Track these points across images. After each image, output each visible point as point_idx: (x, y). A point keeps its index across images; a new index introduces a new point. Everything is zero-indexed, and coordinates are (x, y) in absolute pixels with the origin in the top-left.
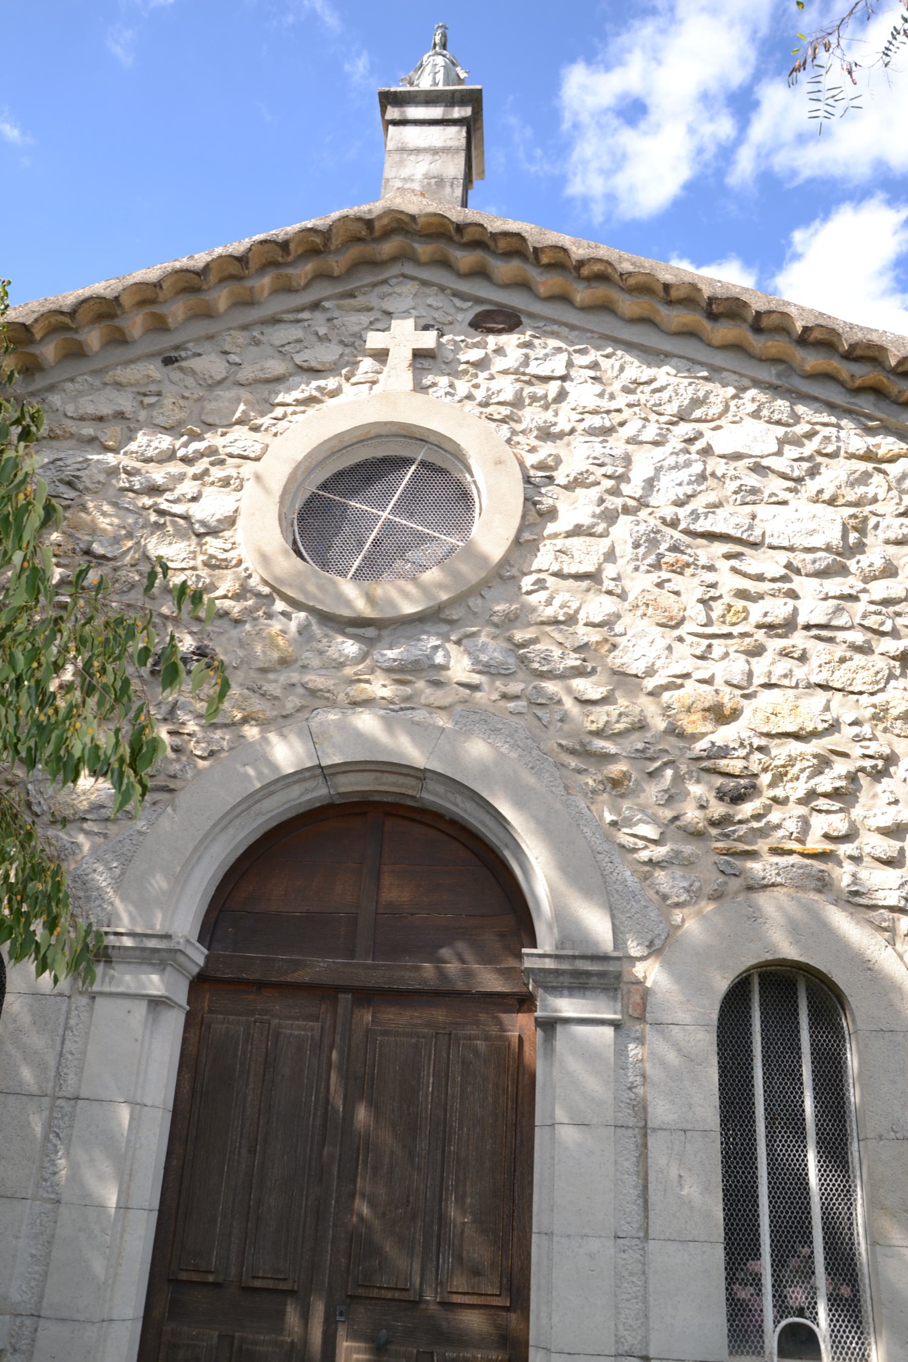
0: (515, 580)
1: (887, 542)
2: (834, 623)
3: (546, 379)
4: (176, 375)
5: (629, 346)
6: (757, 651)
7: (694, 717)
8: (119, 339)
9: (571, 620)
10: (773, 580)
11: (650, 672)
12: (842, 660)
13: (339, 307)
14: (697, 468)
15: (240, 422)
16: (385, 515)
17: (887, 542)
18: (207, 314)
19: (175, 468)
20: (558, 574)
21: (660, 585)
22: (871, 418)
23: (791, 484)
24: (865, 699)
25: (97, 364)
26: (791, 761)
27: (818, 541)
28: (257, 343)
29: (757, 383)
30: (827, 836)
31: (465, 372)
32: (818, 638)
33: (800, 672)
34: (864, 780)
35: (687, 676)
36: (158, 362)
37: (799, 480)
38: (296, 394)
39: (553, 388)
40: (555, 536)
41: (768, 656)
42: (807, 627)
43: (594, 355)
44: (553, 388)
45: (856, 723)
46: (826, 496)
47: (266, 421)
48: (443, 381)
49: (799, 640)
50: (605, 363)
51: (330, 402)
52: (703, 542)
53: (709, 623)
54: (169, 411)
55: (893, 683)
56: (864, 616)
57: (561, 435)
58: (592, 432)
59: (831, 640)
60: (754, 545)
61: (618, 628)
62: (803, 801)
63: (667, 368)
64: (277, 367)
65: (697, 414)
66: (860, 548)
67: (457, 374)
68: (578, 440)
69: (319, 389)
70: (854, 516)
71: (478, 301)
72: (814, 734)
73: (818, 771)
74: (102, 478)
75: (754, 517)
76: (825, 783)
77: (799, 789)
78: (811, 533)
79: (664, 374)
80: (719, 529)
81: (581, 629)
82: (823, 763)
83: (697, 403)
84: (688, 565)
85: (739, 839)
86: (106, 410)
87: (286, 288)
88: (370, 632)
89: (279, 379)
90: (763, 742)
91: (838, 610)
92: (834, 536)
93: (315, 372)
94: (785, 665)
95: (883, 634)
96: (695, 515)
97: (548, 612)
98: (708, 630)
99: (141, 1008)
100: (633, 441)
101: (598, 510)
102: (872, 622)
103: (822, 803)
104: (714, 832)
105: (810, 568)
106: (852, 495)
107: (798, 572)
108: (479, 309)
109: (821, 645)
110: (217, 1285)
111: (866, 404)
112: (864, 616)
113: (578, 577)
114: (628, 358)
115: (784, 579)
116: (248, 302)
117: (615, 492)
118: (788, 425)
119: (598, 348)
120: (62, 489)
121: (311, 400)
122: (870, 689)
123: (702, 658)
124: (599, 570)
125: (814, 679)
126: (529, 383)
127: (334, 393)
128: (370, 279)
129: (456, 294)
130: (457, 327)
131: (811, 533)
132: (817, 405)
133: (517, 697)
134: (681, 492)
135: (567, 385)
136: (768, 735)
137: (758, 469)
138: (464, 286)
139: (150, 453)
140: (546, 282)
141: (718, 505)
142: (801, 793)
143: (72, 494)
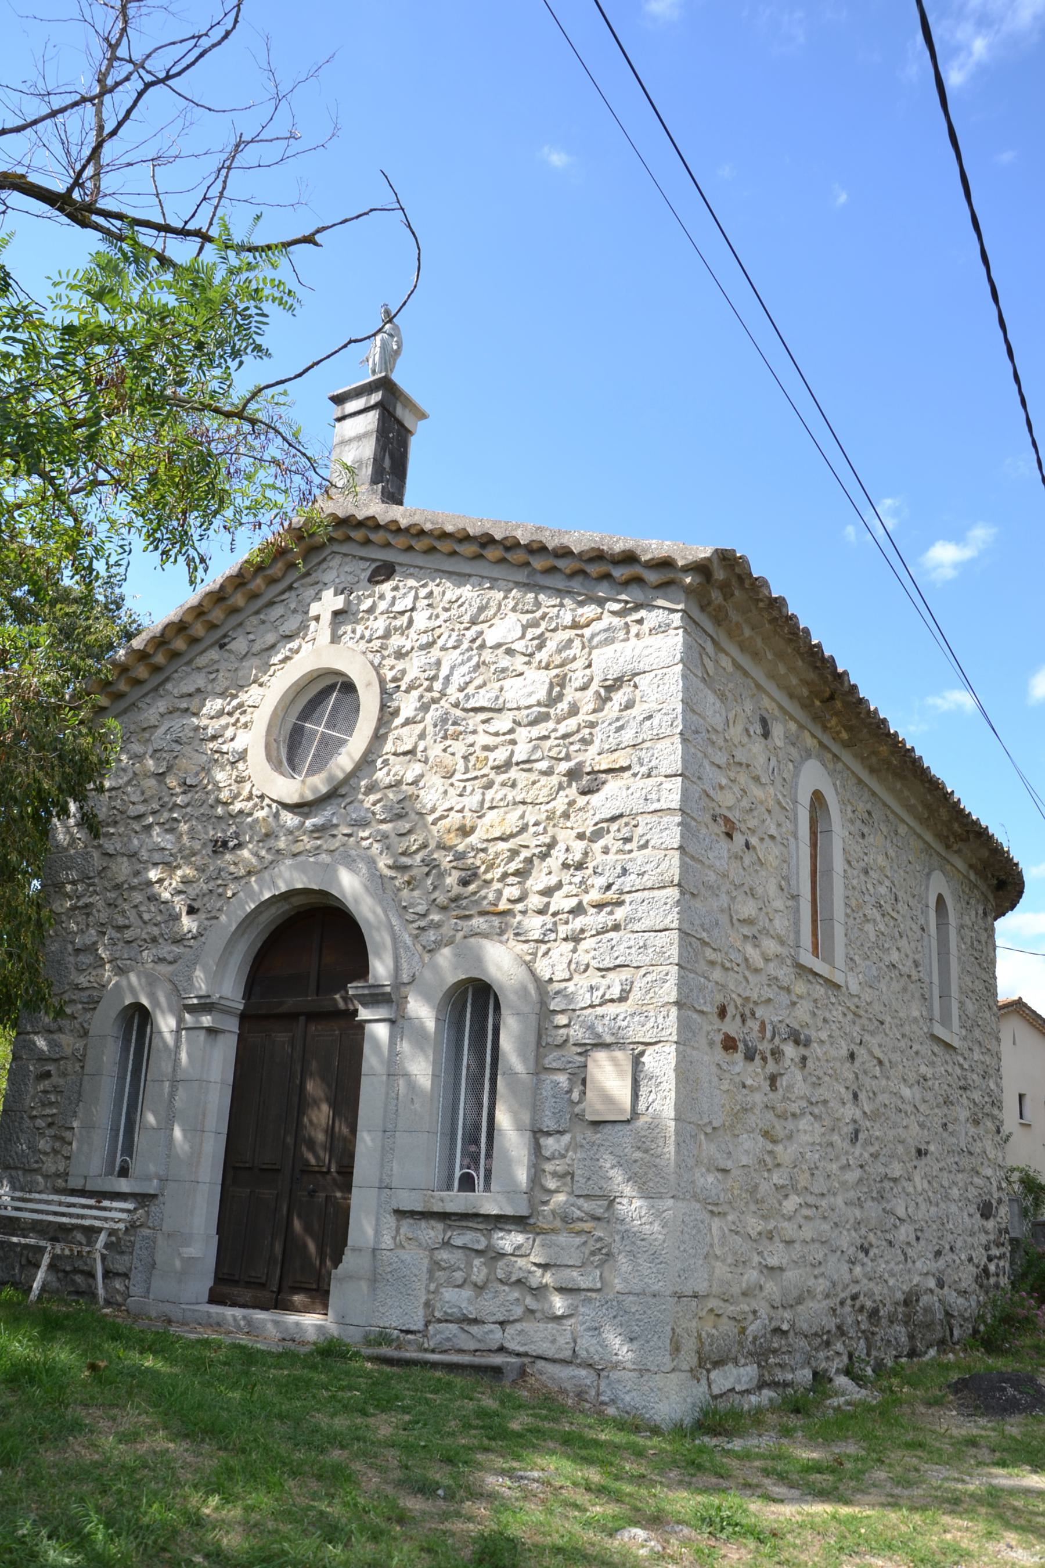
0: (374, 762)
1: (576, 690)
2: (533, 758)
3: (402, 613)
4: (226, 655)
5: (450, 574)
6: (489, 785)
7: (452, 835)
8: (194, 641)
9: (399, 783)
10: (504, 734)
11: (433, 810)
12: (534, 783)
13: (302, 585)
14: (475, 660)
15: (254, 682)
16: (321, 729)
17: (576, 690)
18: (235, 611)
19: (224, 720)
20: (395, 754)
21: (445, 750)
22: (580, 594)
23: (527, 659)
24: (543, 807)
25: (186, 658)
26: (497, 855)
27: (533, 700)
28: (263, 622)
29: (517, 584)
30: (509, 900)
31: (362, 618)
32: (523, 770)
33: (511, 794)
34: (536, 861)
35: (451, 809)
36: (217, 648)
37: (531, 655)
38: (280, 657)
39: (405, 618)
40: (396, 728)
41: (496, 787)
42: (517, 764)
43: (431, 586)
44: (405, 618)
45: (536, 824)
46: (543, 664)
47: (265, 678)
48: (349, 628)
49: (514, 773)
50: (437, 591)
51: (296, 657)
52: (472, 714)
53: (466, 771)
54: (222, 683)
55: (561, 793)
56: (550, 750)
57: (407, 653)
58: (422, 648)
59: (529, 770)
60: (499, 711)
61: (421, 784)
62: (500, 880)
63: (469, 587)
64: (270, 638)
65: (482, 618)
66: (560, 697)
67: (357, 622)
68: (414, 654)
69: (290, 650)
70: (557, 676)
71: (374, 560)
72: (512, 836)
73: (511, 859)
74: (191, 734)
75: (501, 689)
76: (513, 867)
77: (497, 873)
78: (530, 695)
79: (467, 592)
80: (477, 705)
81: (404, 787)
82: (514, 853)
83: (482, 609)
84: (461, 733)
85: (464, 908)
86: (192, 689)
87: (272, 581)
88: (306, 809)
89: (273, 646)
90: (484, 846)
91: (535, 748)
92: (542, 694)
93: (289, 638)
94: (506, 790)
95: (561, 760)
96: (467, 697)
97: (387, 781)
98: (468, 776)
99: (202, 1034)
100: (443, 649)
101: (418, 705)
102: (553, 754)
103: (511, 880)
104: (453, 905)
105: (525, 721)
106: (558, 660)
107: (519, 724)
108: (374, 566)
109: (525, 774)
110: (250, 1169)
111: (576, 585)
112: (550, 750)
113: (405, 754)
114: (448, 584)
115: (511, 731)
116: (254, 596)
117: (430, 689)
118: (533, 612)
119: (433, 580)
120: (174, 745)
121: (287, 659)
122: (546, 799)
123: (461, 795)
124: (415, 747)
125: (518, 799)
126: (395, 618)
127: (297, 651)
128: (316, 561)
129: (362, 558)
130: (362, 584)
131: (530, 695)
132: (549, 592)
133: (367, 838)
134: (462, 681)
135: (414, 614)
136: (488, 840)
137: (510, 652)
138: (363, 552)
139: (213, 713)
140: (400, 542)
141: (485, 684)
142: (498, 876)
143: (179, 748)
